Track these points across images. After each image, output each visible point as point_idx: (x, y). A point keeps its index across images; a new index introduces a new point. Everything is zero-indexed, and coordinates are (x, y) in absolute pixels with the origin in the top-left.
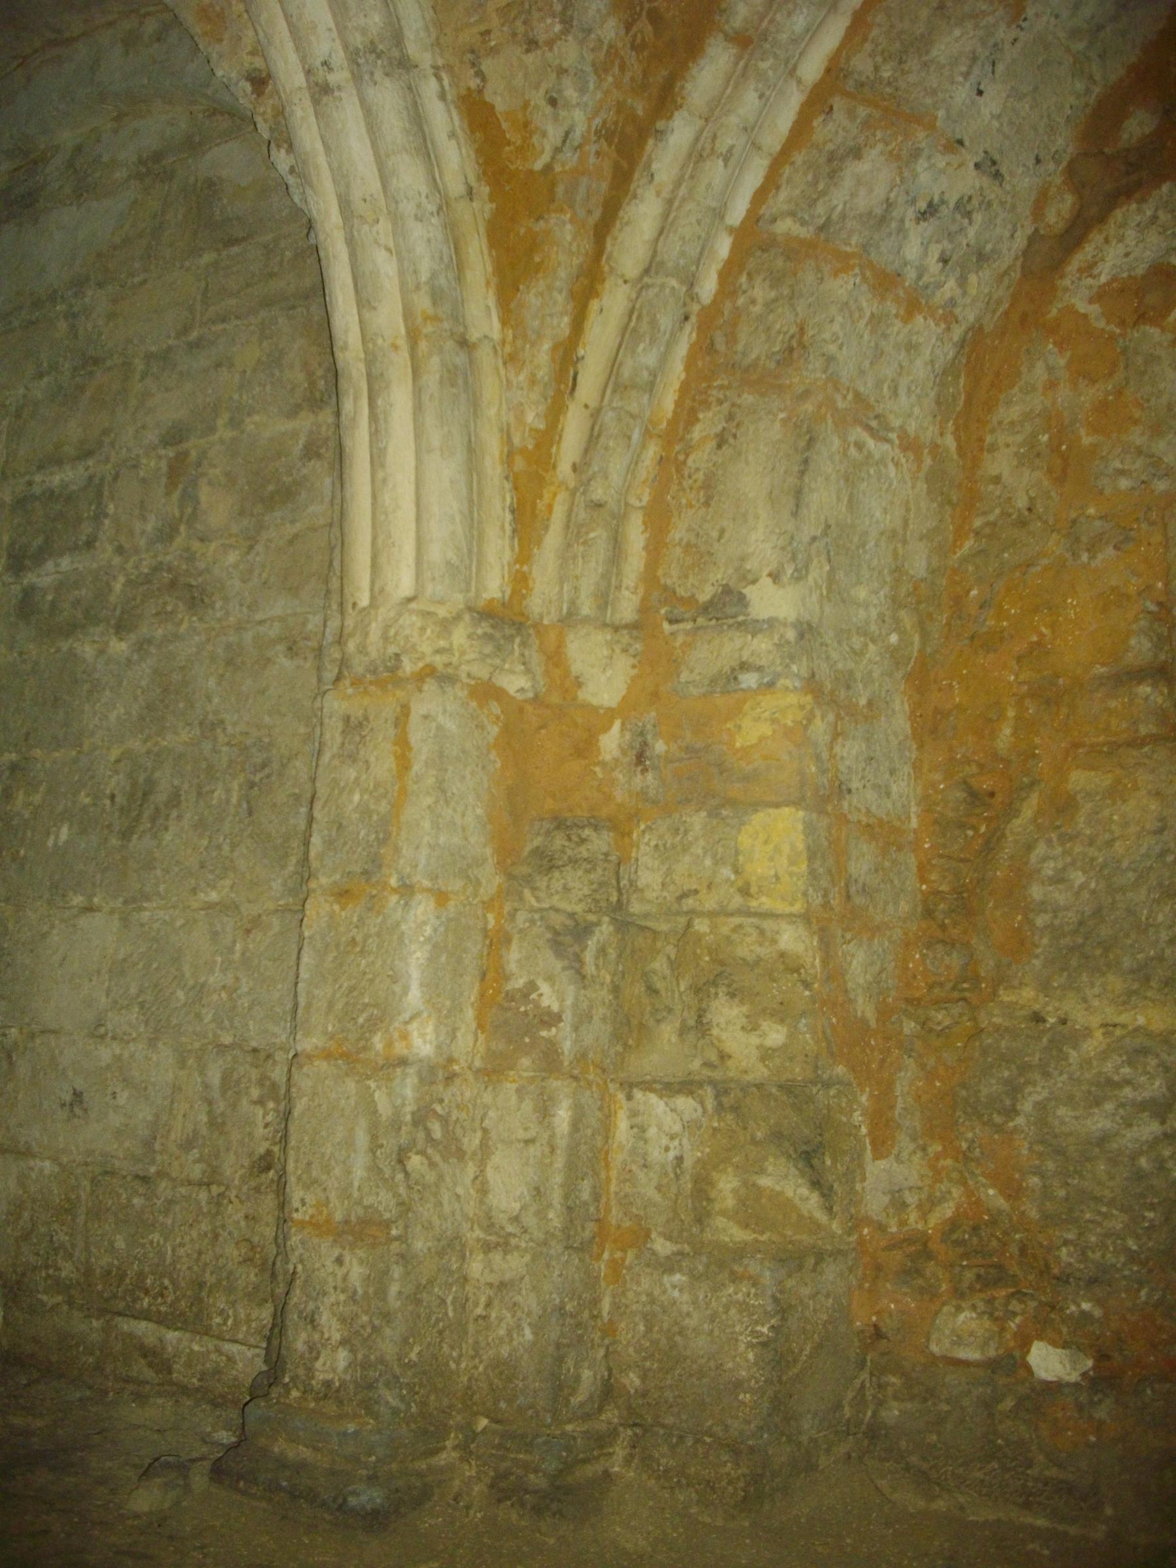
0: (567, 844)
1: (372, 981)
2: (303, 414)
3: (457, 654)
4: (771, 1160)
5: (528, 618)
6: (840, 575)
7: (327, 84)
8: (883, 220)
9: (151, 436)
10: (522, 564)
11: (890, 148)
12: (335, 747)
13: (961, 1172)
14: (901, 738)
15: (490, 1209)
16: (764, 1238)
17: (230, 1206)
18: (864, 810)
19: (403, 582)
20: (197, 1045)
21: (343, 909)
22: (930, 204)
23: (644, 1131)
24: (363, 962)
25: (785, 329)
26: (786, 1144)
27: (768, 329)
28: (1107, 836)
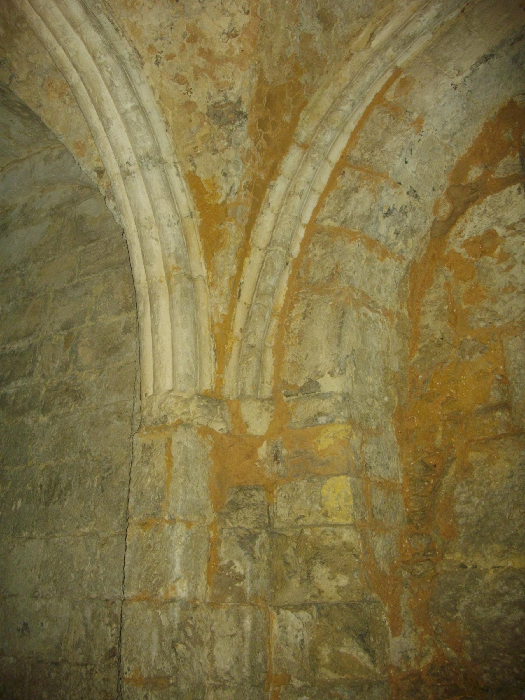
0: (244, 497)
1: (158, 563)
2: (123, 314)
3: (192, 414)
4: (345, 639)
5: (223, 397)
6: (360, 372)
7: (129, 171)
8: (369, 218)
9: (57, 326)
10: (220, 374)
11: (370, 187)
12: (139, 458)
13: (433, 641)
14: (392, 443)
15: (216, 669)
16: (345, 677)
17: (96, 675)
18: (377, 476)
19: (167, 383)
20: (80, 599)
21: (145, 531)
22: (389, 210)
23: (285, 629)
24: (154, 555)
25: (330, 266)
26: (352, 632)
27: (323, 267)
28: (488, 481)
